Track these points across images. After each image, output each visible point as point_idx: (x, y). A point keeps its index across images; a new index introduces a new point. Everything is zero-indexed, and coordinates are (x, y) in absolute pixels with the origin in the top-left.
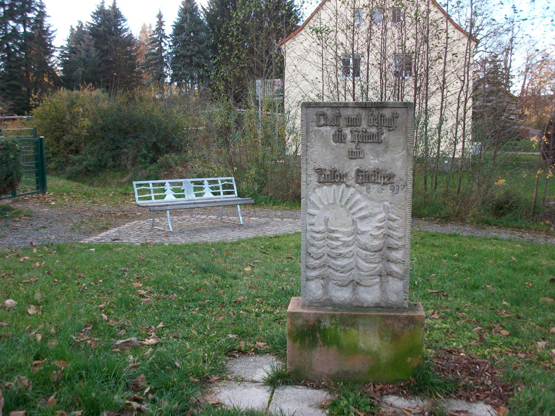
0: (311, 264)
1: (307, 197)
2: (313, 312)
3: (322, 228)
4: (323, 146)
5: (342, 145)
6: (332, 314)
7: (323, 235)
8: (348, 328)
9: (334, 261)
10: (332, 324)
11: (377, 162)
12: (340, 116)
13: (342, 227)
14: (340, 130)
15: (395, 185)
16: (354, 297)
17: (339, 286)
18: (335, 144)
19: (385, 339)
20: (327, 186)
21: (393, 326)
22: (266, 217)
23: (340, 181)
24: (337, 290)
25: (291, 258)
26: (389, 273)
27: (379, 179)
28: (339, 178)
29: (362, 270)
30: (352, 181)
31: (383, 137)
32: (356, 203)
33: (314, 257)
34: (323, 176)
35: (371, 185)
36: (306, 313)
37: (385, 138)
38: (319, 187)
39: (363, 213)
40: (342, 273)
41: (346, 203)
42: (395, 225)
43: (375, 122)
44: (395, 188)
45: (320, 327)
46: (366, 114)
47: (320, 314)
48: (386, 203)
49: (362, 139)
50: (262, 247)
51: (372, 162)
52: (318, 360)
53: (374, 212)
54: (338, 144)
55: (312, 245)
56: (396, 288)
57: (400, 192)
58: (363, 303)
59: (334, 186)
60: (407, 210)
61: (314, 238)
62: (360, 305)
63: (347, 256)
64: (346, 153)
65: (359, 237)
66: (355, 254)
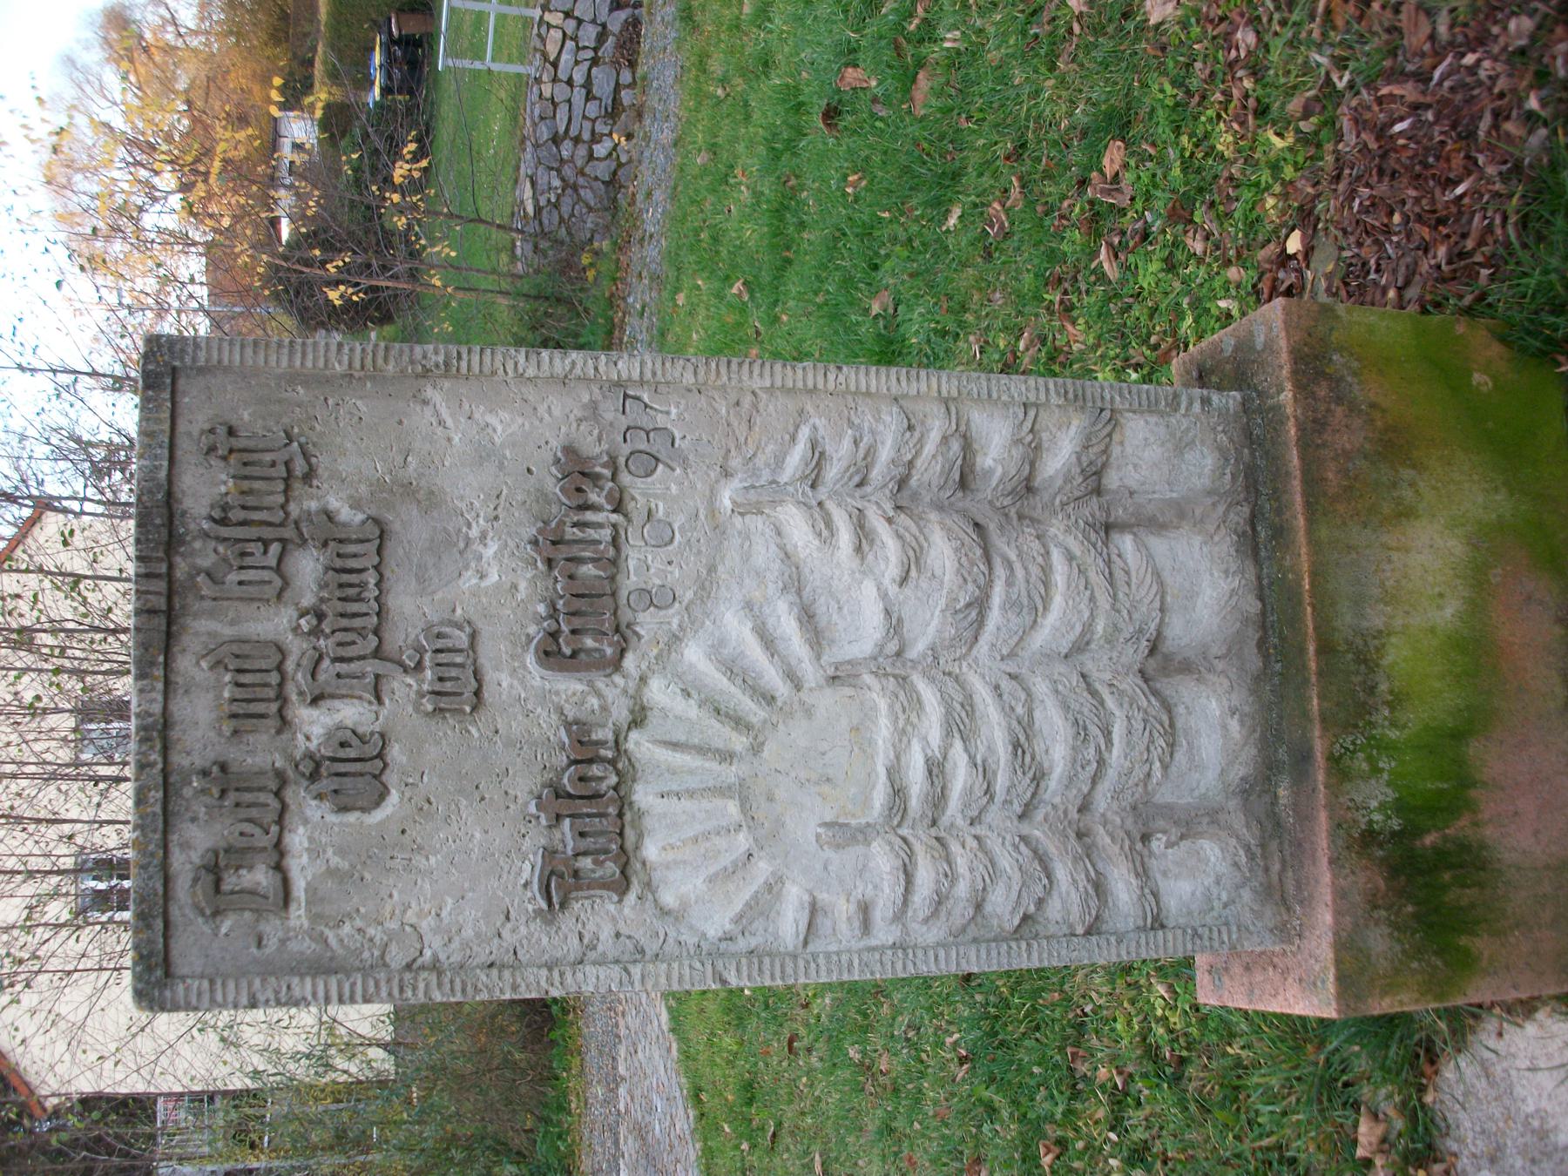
0: (1076, 911)
1: (715, 954)
2: (1326, 878)
3: (882, 859)
4: (408, 868)
5: (396, 753)
6: (1328, 773)
7: (918, 848)
8: (1383, 687)
9: (1053, 783)
10: (1376, 770)
11: (490, 550)
12: (223, 767)
13: (871, 742)
14: (306, 768)
15: (626, 449)
16: (1220, 665)
17: (1172, 745)
18: (394, 797)
19: (1407, 494)
20: (640, 836)
21: (1347, 455)
22: (616, 1134)
23: (613, 762)
24: (1191, 760)
25: (791, 1042)
26: (1092, 482)
27: (592, 533)
28: (596, 770)
29: (1088, 628)
30: (610, 694)
31: (345, 514)
32: (733, 668)
33: (1039, 891)
34: (586, 863)
35: (630, 581)
36: (1338, 914)
37: (356, 505)
38: (648, 885)
39: (787, 625)
40: (1107, 734)
41: (739, 722)
42: (841, 453)
43: (257, 559)
44: (643, 446)
45: (1394, 834)
46: (211, 614)
47: (1332, 837)
48: (726, 501)
49: (360, 632)
50: (745, 1146)
51: (493, 577)
52: (1536, 833)
53: (777, 565)
54: (391, 778)
55: (979, 907)
56: (1154, 453)
57: (661, 421)
58: (1246, 621)
59: (643, 795)
60: (757, 383)
61: (940, 900)
62: (1253, 635)
63: (1020, 710)
64: (448, 730)
65: (918, 649)
66: (1011, 667)
